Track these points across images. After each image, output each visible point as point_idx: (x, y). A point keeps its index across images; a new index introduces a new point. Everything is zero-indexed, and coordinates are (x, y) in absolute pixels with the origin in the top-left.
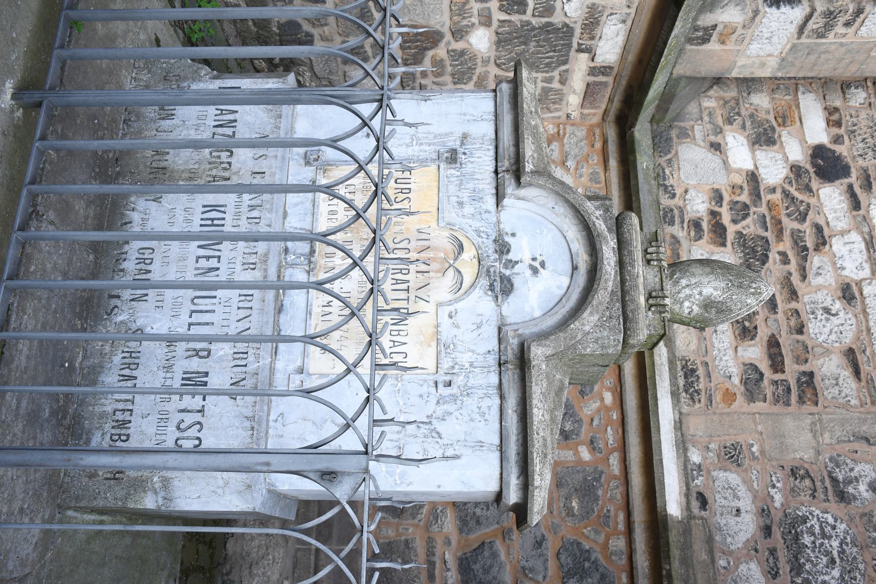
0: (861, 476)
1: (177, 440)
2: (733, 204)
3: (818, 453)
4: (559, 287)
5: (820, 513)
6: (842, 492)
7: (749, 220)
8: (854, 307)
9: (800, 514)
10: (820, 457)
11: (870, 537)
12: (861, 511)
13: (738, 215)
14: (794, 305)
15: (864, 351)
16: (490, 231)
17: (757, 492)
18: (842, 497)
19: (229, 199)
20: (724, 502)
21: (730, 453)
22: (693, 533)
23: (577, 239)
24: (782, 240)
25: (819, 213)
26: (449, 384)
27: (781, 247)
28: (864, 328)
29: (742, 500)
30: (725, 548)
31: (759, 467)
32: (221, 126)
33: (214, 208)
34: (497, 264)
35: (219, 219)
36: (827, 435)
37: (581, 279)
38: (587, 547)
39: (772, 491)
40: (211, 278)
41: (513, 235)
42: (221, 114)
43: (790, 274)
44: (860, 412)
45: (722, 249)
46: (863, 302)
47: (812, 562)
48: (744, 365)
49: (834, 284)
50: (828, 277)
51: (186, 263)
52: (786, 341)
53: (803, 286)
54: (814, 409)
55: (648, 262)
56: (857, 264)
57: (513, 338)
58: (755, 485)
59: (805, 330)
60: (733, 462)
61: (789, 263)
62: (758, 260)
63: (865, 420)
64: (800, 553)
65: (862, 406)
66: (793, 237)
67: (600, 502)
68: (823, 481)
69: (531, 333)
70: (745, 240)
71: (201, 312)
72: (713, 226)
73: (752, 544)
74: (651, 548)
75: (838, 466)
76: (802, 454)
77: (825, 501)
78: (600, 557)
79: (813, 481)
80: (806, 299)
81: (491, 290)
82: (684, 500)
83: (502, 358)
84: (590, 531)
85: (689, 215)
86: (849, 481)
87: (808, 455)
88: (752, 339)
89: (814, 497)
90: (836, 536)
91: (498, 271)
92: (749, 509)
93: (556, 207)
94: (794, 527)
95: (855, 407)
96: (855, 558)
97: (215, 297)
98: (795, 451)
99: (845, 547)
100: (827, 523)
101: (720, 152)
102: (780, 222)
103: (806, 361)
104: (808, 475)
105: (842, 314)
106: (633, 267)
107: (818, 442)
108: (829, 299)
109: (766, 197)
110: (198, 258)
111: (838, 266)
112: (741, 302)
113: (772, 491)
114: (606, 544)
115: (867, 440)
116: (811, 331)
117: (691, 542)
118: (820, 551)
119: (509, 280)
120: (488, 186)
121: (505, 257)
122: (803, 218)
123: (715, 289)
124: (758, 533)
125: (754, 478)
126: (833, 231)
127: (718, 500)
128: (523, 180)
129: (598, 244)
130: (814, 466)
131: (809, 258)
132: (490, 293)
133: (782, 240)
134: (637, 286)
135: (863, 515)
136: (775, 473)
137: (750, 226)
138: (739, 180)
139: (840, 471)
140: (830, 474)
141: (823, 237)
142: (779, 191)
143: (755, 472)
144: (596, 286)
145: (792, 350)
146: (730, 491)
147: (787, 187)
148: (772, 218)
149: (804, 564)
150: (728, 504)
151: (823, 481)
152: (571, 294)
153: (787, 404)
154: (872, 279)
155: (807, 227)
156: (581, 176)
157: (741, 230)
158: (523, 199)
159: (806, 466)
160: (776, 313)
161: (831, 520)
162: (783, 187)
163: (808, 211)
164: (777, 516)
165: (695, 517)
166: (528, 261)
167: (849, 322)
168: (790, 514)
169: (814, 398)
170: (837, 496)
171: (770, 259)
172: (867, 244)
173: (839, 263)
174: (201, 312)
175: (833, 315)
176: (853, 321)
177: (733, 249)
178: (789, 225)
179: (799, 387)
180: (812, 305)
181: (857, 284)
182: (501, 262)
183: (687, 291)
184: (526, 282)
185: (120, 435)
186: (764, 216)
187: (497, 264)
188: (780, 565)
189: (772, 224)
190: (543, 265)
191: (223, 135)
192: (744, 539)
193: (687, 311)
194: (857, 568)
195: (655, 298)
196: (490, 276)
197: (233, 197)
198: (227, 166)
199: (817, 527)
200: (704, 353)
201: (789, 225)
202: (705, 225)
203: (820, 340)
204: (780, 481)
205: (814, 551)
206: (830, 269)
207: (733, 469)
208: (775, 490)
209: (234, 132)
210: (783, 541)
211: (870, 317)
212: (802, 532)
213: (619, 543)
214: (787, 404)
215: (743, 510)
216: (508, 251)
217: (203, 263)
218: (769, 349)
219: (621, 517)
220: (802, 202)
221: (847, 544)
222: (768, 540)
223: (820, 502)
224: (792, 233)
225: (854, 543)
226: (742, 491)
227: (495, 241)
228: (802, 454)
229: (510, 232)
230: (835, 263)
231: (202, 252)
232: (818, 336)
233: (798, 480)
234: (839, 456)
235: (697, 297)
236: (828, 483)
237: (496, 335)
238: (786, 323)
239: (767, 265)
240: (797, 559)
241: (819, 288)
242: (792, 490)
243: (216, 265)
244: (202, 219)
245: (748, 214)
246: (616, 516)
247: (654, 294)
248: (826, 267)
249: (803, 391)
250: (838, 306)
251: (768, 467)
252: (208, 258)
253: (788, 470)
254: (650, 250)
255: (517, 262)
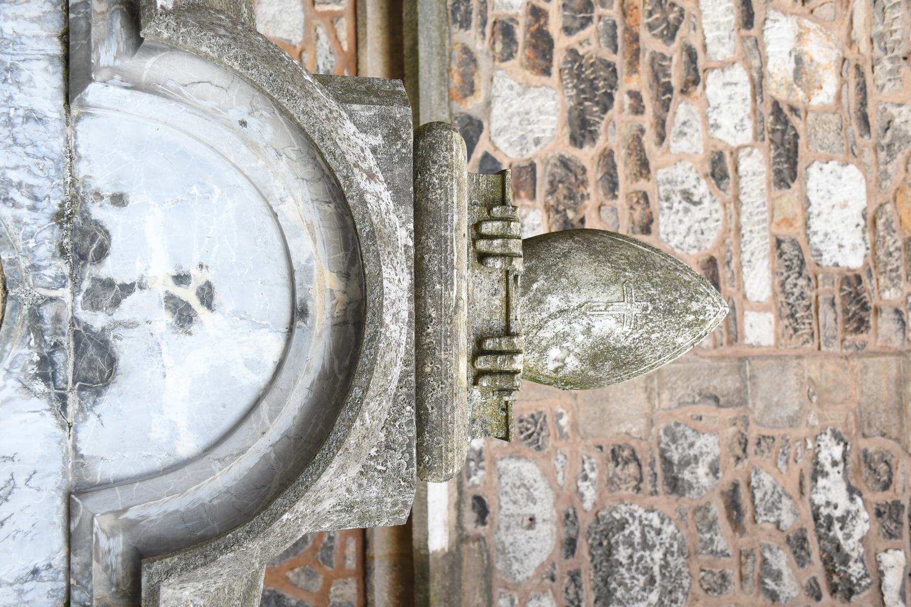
0: (701, 454)
3: (651, 423)
4: (251, 365)
5: (649, 516)
6: (676, 479)
7: (590, 30)
8: (724, 190)
9: (617, 516)
10: (654, 430)
11: (701, 540)
12: (695, 504)
13: (574, 18)
14: (642, 185)
15: (728, 263)
16: (42, 185)
17: (561, 488)
18: (675, 485)
20: (513, 509)
21: (527, 429)
22: (465, 564)
23: (310, 227)
24: (636, 72)
25: (695, 29)
28: (733, 226)
29: (539, 504)
30: (509, 580)
31: (567, 450)
34: (65, 293)
36: (665, 395)
37: (316, 347)
39: (583, 486)
41: (119, 200)
43: (642, 131)
44: (711, 357)
45: (544, 79)
46: (737, 184)
47: (626, 585)
49: (701, 152)
50: (694, 139)
53: (659, 153)
55: (482, 258)
56: (737, 121)
57: (111, 535)
59: (653, 227)
60: (530, 444)
61: (642, 113)
62: (597, 104)
63: (717, 370)
64: (610, 574)
65: (715, 347)
66: (652, 67)
68: (652, 465)
69: (167, 515)
70: (581, 66)
72: (533, 36)
73: (548, 569)
74: (398, 598)
75: (674, 440)
76: (630, 425)
77: (651, 494)
79: (640, 466)
80: (660, 175)
81: (45, 378)
82: (454, 513)
83: (76, 594)
84: (298, 575)
85: (496, 12)
86: (686, 463)
87: (636, 427)
90: (661, 544)
91: (67, 316)
92: (547, 516)
93: (252, 122)
94: (606, 536)
95: (708, 349)
96: (680, 572)
98: (620, 422)
99: (669, 558)
100: (651, 526)
102: (636, 39)
104: (634, 457)
105: (706, 202)
106: (447, 282)
107: (653, 407)
108: (693, 176)
111: (711, 122)
112: (665, 344)
113: (583, 486)
115: (716, 399)
116: (662, 228)
117: (460, 580)
118: (637, 569)
119: (103, 346)
120: (36, 29)
121: (90, 271)
122: (670, 33)
123: (620, 320)
124: (558, 551)
125: (559, 466)
126: (710, 61)
127: (504, 506)
128: (147, 32)
129: (369, 257)
130: (643, 444)
131: (672, 105)
132: (39, 386)
133: (636, 72)
134: (452, 335)
135: (698, 509)
136: (589, 458)
139: (676, 448)
140: (663, 453)
141: (696, 70)
143: (561, 458)
144: (357, 392)
146: (523, 490)
148: (627, 29)
149: (615, 589)
150: (518, 511)
151: (652, 465)
152: (287, 393)
154: (753, 147)
155: (674, 51)
157: (577, 47)
158: (148, 88)
159: (633, 443)
160: (615, 197)
161: (656, 522)
163: (680, 22)
164: (585, 521)
165: (467, 537)
166: (162, 284)
167: (715, 216)
168: (604, 517)
170: (668, 484)
171: (616, 104)
172: (754, 87)
173: (713, 116)
175: (695, 204)
176: (721, 213)
177: (561, 80)
178: (651, 44)
180: (668, 187)
181: (732, 153)
182: (76, 286)
183: (559, 325)
184: (155, 350)
186: (614, 26)
187: (65, 293)
188: (583, 595)
189: (624, 40)
190: (207, 295)
192: (537, 563)
193: (551, 366)
194: (681, 586)
195: (492, 348)
196: (40, 333)
199: (638, 534)
201: (651, 44)
202: (520, 33)
203: (673, 244)
204: (595, 467)
205: (629, 570)
206: (700, 127)
207: (530, 455)
208: (588, 483)
210: (589, 558)
211: (744, 208)
212: (617, 543)
215: (539, 519)
216: (102, 253)
221: (672, 554)
222: (571, 560)
223: (645, 496)
224: (653, 59)
225: (681, 552)
226: (541, 490)
227: (59, 217)
228: (630, 425)
229: (107, 191)
230: (706, 117)
232: (671, 237)
233: (620, 467)
234: (677, 424)
235: (580, 338)
236: (658, 469)
237: (59, 518)
238: (627, 215)
239: (610, 112)
240: (606, 583)
241: (680, 158)
242: (611, 481)
245: (589, 20)
246: (344, 546)
247: (489, 344)
248: (695, 123)
250: (702, 189)
251: (580, 449)
253: (607, 451)
254: (488, 228)
255: (127, 289)
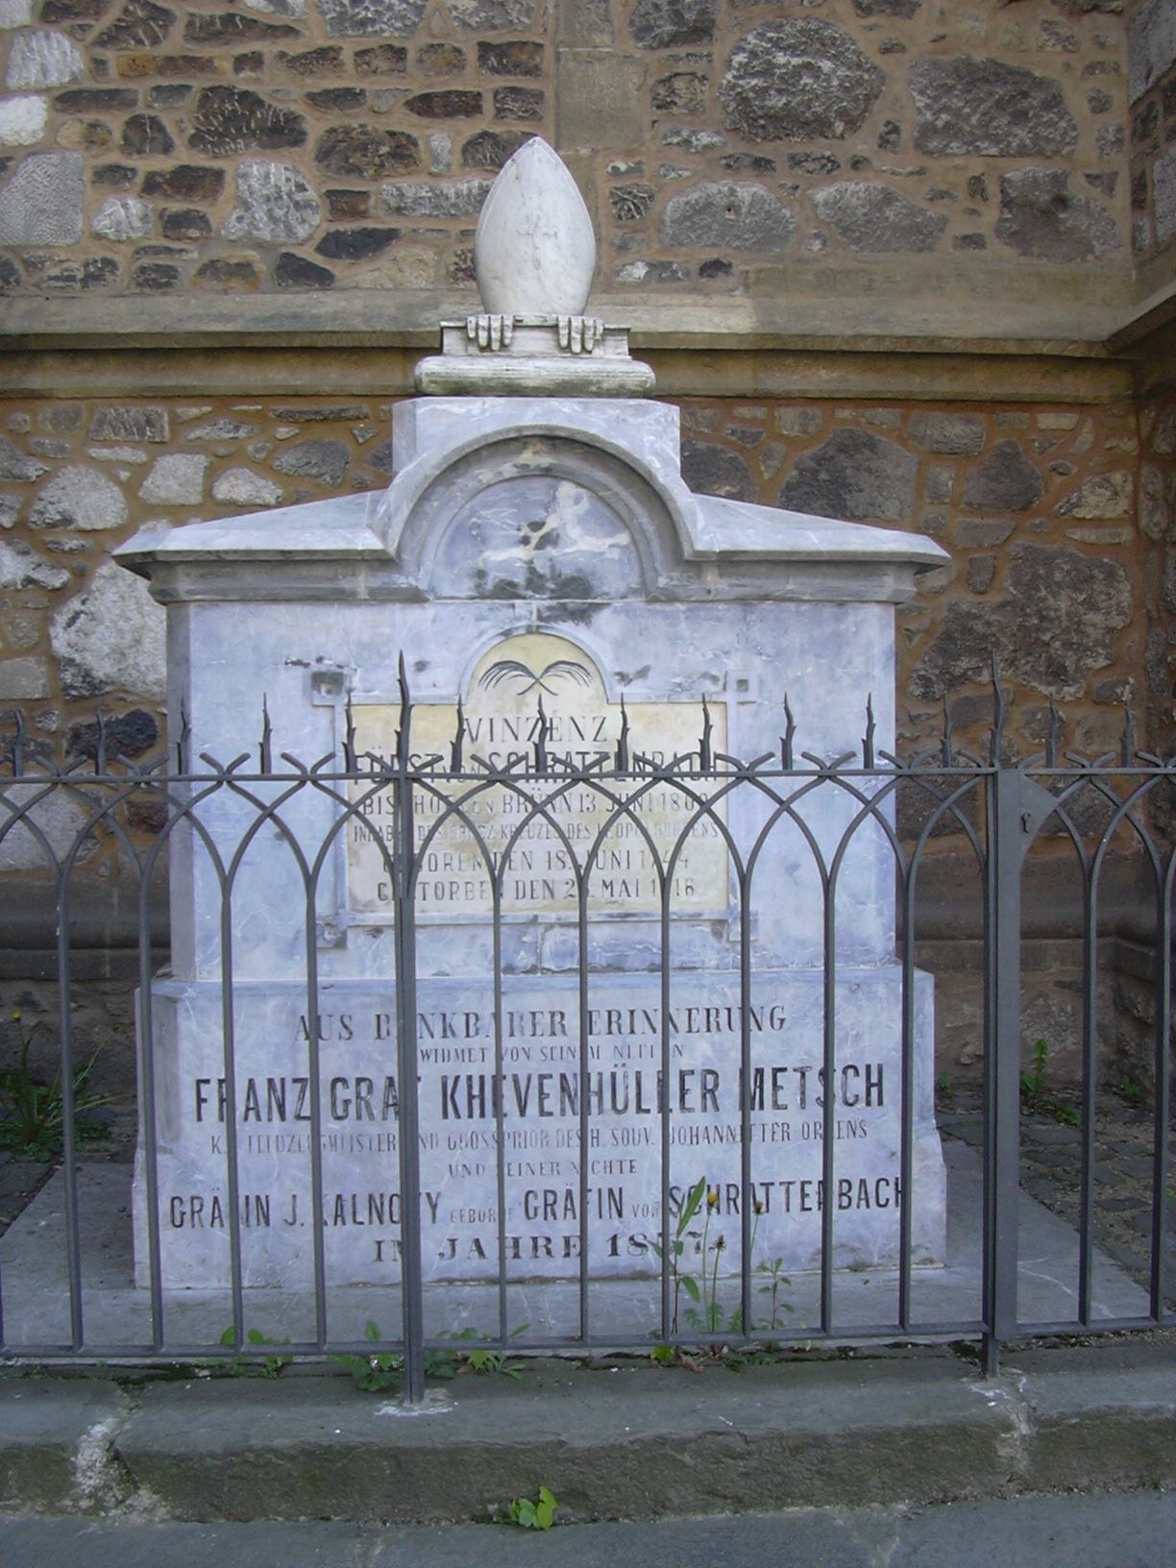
1: (848, 1104)
2: (129, 146)
4: (577, 501)
9: (733, 105)
13: (153, 139)
19: (430, 1076)
26: (743, 684)
27: (227, 66)
32: (281, 1108)
33: (448, 1096)
35: (470, 1087)
37: (570, 461)
38: (795, 473)
40: (574, 1085)
42: (256, 1109)
45: (228, 178)
48: (465, 163)
51: (552, 1132)
52: (417, 84)
54: (549, 52)
58: (686, 174)
62: (253, 113)
67: (719, 447)
70: (209, 132)
71: (639, 1094)
78: (807, 452)
87: (633, 77)
88: (415, 144)
89: (704, 78)
97: (613, 1075)
101: (9, 159)
103: (459, 51)
109: (113, 81)
110: (542, 1113)
114: (788, 440)
137: (178, 119)
138: (72, 129)
142: (100, 53)
145: (438, 74)
147: (92, 35)
148: (161, 71)
153: (539, 96)
156: (61, 449)
159: (651, 81)
161: (741, 58)
162: (94, 44)
169: (530, 48)
171: (251, 88)
174: (639, 1094)
178: (175, 42)
179: (509, 72)
185: (841, 1195)
186: (157, 88)
190: (536, 526)
191: (302, 1098)
194: (816, 32)
197: (424, 1068)
198: (364, 1086)
200: (440, 236)
202: (176, 206)
209: (295, 1081)
213: (788, 419)
214: (539, 96)
216: (511, 584)
217: (552, 1104)
218: (435, 115)
219: (744, 411)
220: (126, 11)
222: (776, 165)
231: (532, 1108)
238: (384, 78)
239: (262, 96)
240: (807, 123)
242: (693, 112)
243: (557, 1079)
244: (471, 1116)
246: (742, 420)
249: (517, 66)
252: (542, 1096)
254: (483, 342)
